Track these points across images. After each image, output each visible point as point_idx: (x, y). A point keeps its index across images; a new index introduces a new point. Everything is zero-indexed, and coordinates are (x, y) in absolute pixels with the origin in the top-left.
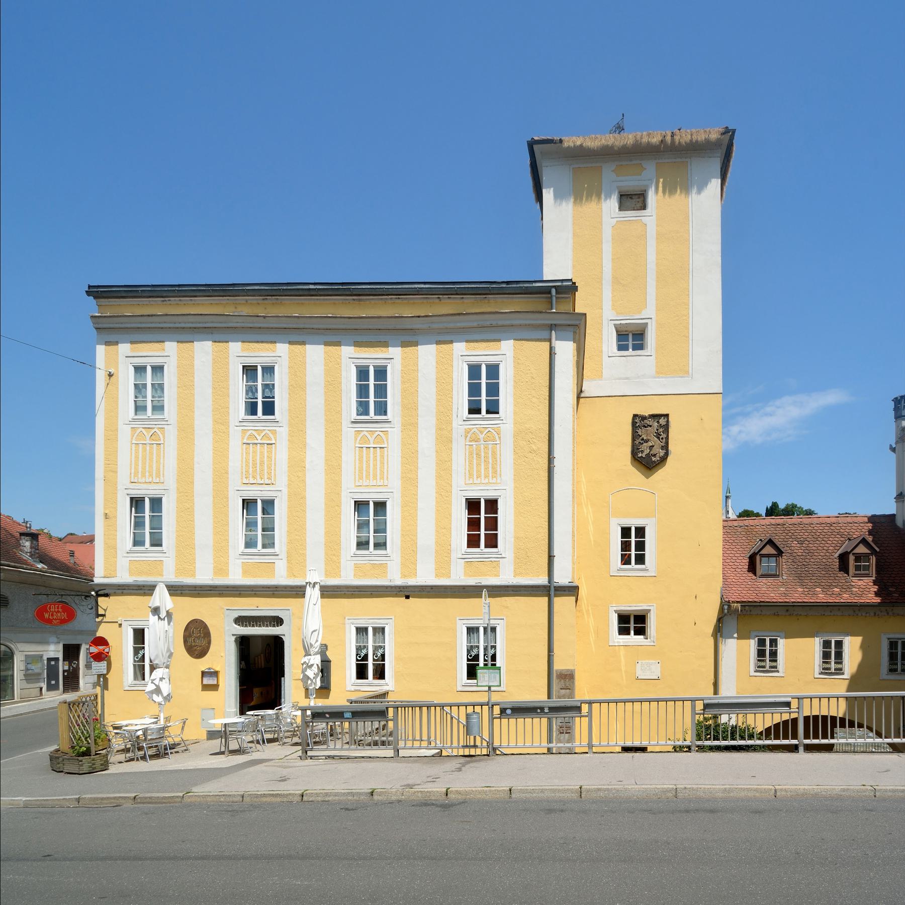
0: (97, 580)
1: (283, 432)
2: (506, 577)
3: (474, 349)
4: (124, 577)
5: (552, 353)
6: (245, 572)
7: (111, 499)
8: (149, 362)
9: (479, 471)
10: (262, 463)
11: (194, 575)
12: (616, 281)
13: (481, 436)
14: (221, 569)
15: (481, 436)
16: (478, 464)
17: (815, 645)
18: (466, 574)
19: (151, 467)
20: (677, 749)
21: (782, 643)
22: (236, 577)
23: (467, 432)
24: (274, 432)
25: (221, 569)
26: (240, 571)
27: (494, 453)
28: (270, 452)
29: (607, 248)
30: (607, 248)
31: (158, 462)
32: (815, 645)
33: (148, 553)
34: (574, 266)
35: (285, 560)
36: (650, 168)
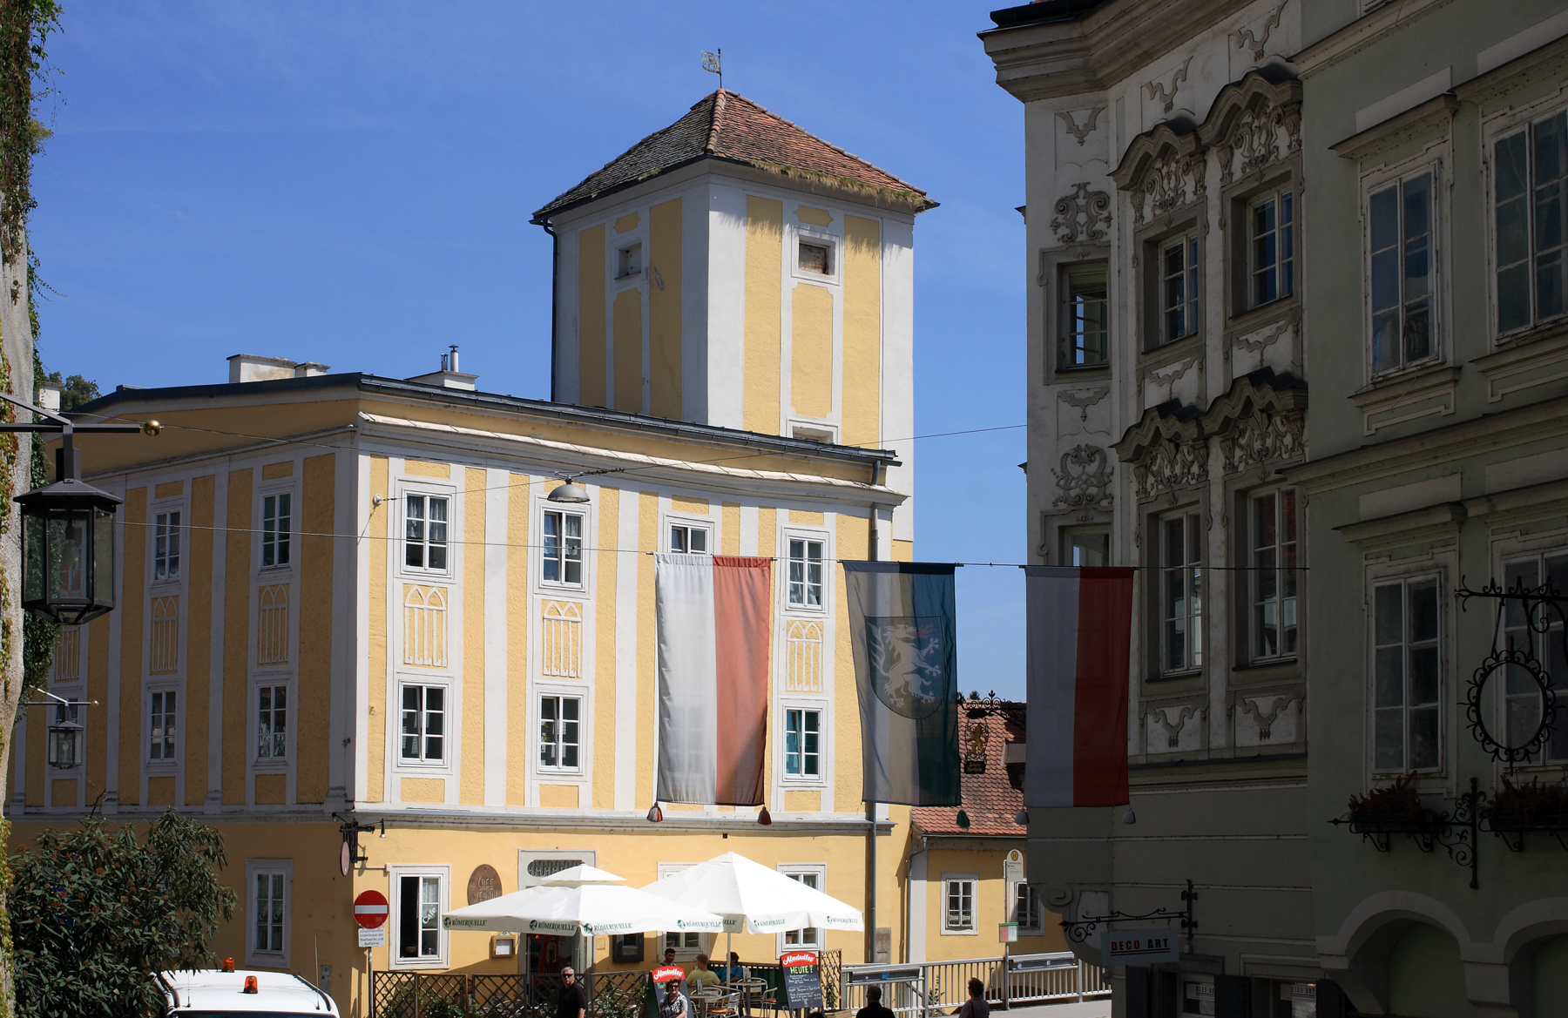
0: (360, 807)
1: (590, 605)
2: (827, 812)
3: (797, 521)
4: (394, 803)
5: (873, 534)
6: (544, 800)
7: (379, 687)
8: (428, 492)
9: (800, 676)
10: (566, 646)
11: (482, 802)
12: (797, 367)
13: (804, 632)
14: (515, 793)
15: (804, 632)
16: (800, 667)
17: (942, 887)
18: (787, 808)
19: (431, 643)
20: (1290, 983)
21: (975, 884)
22: (533, 806)
23: (790, 624)
24: (580, 606)
25: (515, 793)
26: (536, 797)
27: (816, 653)
28: (575, 633)
29: (787, 317)
30: (787, 317)
31: (440, 637)
32: (942, 887)
33: (423, 767)
34: (746, 334)
35: (590, 784)
36: (838, 215)
